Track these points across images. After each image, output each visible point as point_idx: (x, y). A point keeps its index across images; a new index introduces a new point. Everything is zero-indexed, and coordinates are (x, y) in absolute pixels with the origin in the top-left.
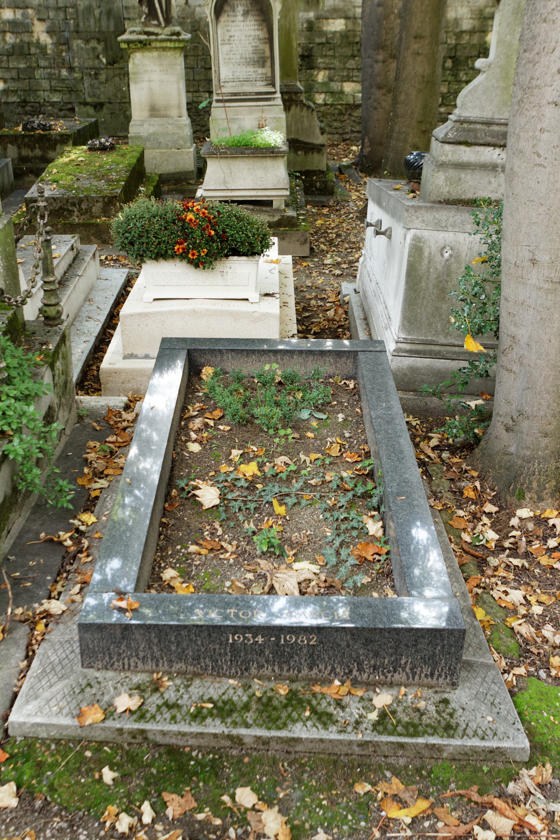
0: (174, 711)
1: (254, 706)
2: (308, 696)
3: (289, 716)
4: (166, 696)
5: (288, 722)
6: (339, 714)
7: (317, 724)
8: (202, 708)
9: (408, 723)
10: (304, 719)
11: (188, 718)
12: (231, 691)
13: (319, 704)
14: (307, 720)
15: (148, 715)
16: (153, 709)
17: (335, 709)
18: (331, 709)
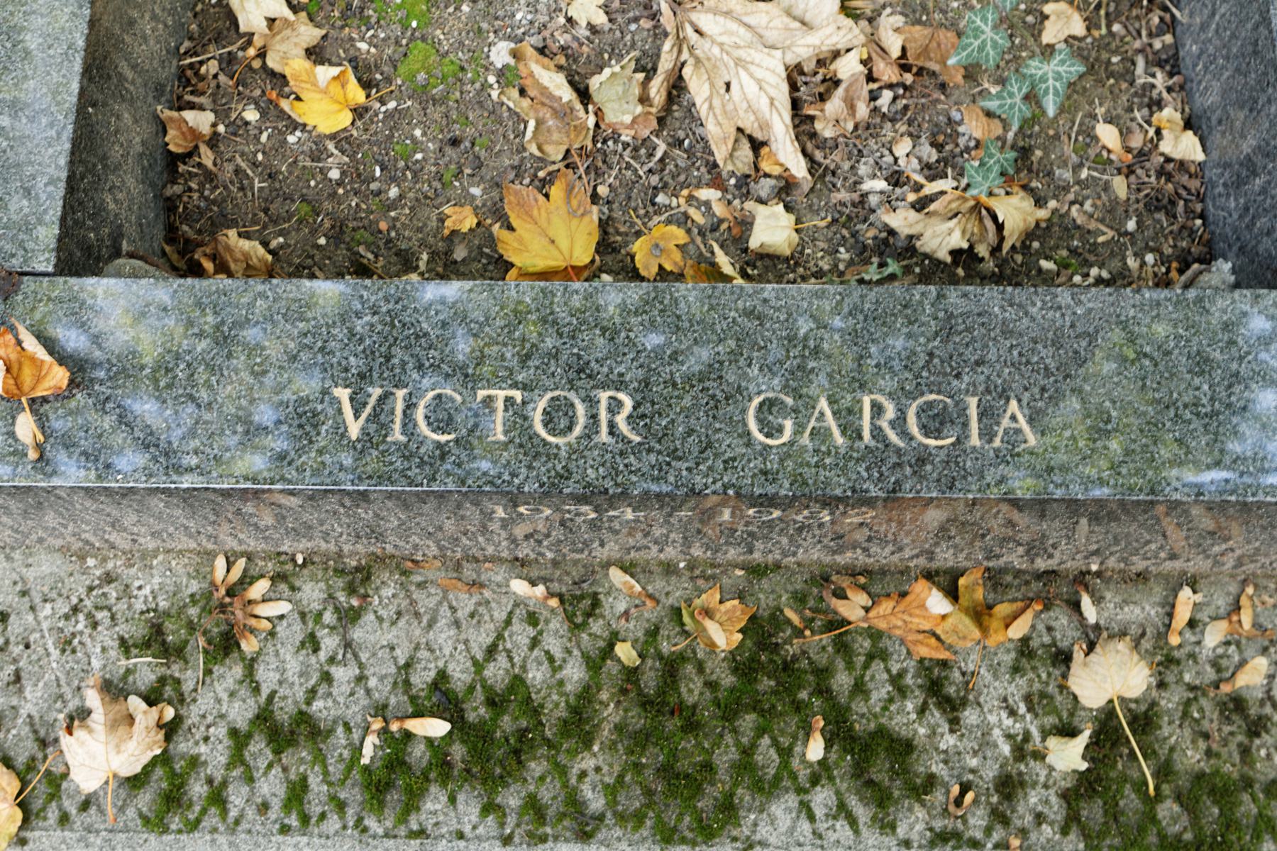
0: (299, 759)
1: (610, 713)
2: (818, 643)
3: (745, 764)
4: (267, 676)
5: (743, 794)
6: (939, 744)
7: (853, 802)
8: (408, 736)
9: (1200, 777)
10: (803, 774)
11: (352, 794)
12: (521, 634)
13: (859, 688)
14: (815, 780)
15: (198, 789)
16: (216, 756)
17: (922, 711)
18: (906, 718)
